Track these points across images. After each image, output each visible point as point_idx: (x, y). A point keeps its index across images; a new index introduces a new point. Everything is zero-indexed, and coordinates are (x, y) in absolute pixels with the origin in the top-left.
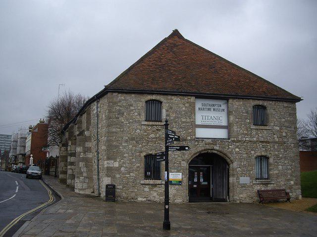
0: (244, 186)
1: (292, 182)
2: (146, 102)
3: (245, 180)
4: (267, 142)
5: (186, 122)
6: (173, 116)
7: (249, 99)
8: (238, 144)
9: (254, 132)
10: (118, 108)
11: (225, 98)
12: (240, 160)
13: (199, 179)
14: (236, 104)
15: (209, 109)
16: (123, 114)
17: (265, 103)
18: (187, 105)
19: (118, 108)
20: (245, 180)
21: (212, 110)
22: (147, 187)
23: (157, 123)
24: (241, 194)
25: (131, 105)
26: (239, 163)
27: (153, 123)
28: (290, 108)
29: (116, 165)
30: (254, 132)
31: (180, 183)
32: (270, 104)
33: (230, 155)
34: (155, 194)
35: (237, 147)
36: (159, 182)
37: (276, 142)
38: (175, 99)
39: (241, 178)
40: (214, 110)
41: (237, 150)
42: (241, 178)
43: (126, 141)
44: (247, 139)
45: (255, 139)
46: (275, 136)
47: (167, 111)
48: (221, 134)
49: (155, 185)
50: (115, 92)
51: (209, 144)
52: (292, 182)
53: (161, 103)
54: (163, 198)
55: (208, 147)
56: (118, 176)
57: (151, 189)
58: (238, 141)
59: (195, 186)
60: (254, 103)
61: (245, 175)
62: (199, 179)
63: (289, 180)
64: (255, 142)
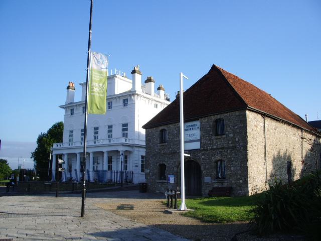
0: (207, 184)
1: (241, 181)
4: (223, 148)
6: (171, 137)
17: (222, 116)
28: (241, 116)
33: (198, 161)
35: (203, 154)
37: (229, 148)
41: (203, 157)
44: (210, 148)
45: (215, 147)
46: (230, 142)
47: (168, 135)
50: (154, 127)
52: (241, 181)
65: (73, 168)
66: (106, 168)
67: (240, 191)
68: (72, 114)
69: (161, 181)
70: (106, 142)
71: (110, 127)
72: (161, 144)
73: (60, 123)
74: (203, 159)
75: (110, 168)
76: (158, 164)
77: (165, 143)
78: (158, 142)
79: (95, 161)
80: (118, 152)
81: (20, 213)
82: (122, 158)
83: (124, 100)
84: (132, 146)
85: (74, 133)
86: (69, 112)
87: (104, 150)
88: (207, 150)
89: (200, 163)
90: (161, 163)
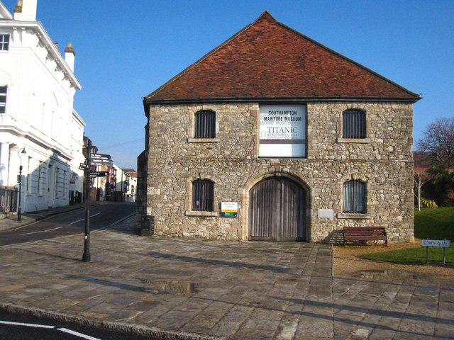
6: (228, 129)
10: (160, 123)
16: (166, 130)
19: (160, 123)
21: (283, 120)
22: (195, 219)
23: (208, 140)
25: (177, 119)
27: (202, 140)
29: (158, 192)
36: (208, 213)
47: (220, 124)
49: (203, 218)
51: (276, 165)
56: (159, 206)
58: (317, 160)
61: (324, 206)
63: (395, 215)
67: (398, 234)
78: (193, 136)
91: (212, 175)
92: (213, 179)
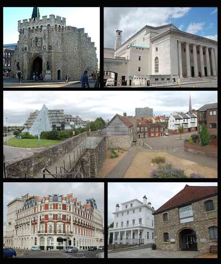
0: (203, 243)
2: (205, 203)
3: (203, 240)
5: (175, 218)
6: (171, 217)
7: (201, 200)
8: (197, 223)
9: (206, 215)
11: (189, 204)
12: (200, 230)
13: (193, 240)
14: (195, 204)
15: (184, 211)
18: (175, 212)
20: (203, 240)
24: (202, 247)
26: (199, 232)
27: (211, 211)
30: (206, 215)
31: (174, 243)
32: (214, 198)
34: (167, 247)
35: (197, 224)
38: (171, 211)
39: (201, 239)
40: (186, 210)
41: (197, 225)
42: (201, 239)
43: (158, 229)
45: (207, 218)
48: (191, 220)
53: (212, 201)
54: (102, 244)
55: (184, 227)
57: (166, 245)
59: (191, 243)
60: (204, 201)
61: (202, 238)
62: (193, 240)
64: (207, 220)
65: (123, 237)
66: (132, 237)
68: (117, 216)
69: (165, 243)
70: (132, 226)
71: (128, 221)
72: (164, 222)
73: (153, 250)
74: (198, 227)
75: (133, 238)
76: (163, 233)
77: (167, 220)
78: (162, 220)
79: (127, 234)
80: (137, 230)
81: (147, 236)
82: (139, 233)
83: (140, 209)
84: (143, 228)
85: (118, 224)
86: (117, 216)
87: (131, 229)
88: (201, 221)
89: (195, 230)
90: (165, 232)
91: (167, 231)
92: (168, 233)
